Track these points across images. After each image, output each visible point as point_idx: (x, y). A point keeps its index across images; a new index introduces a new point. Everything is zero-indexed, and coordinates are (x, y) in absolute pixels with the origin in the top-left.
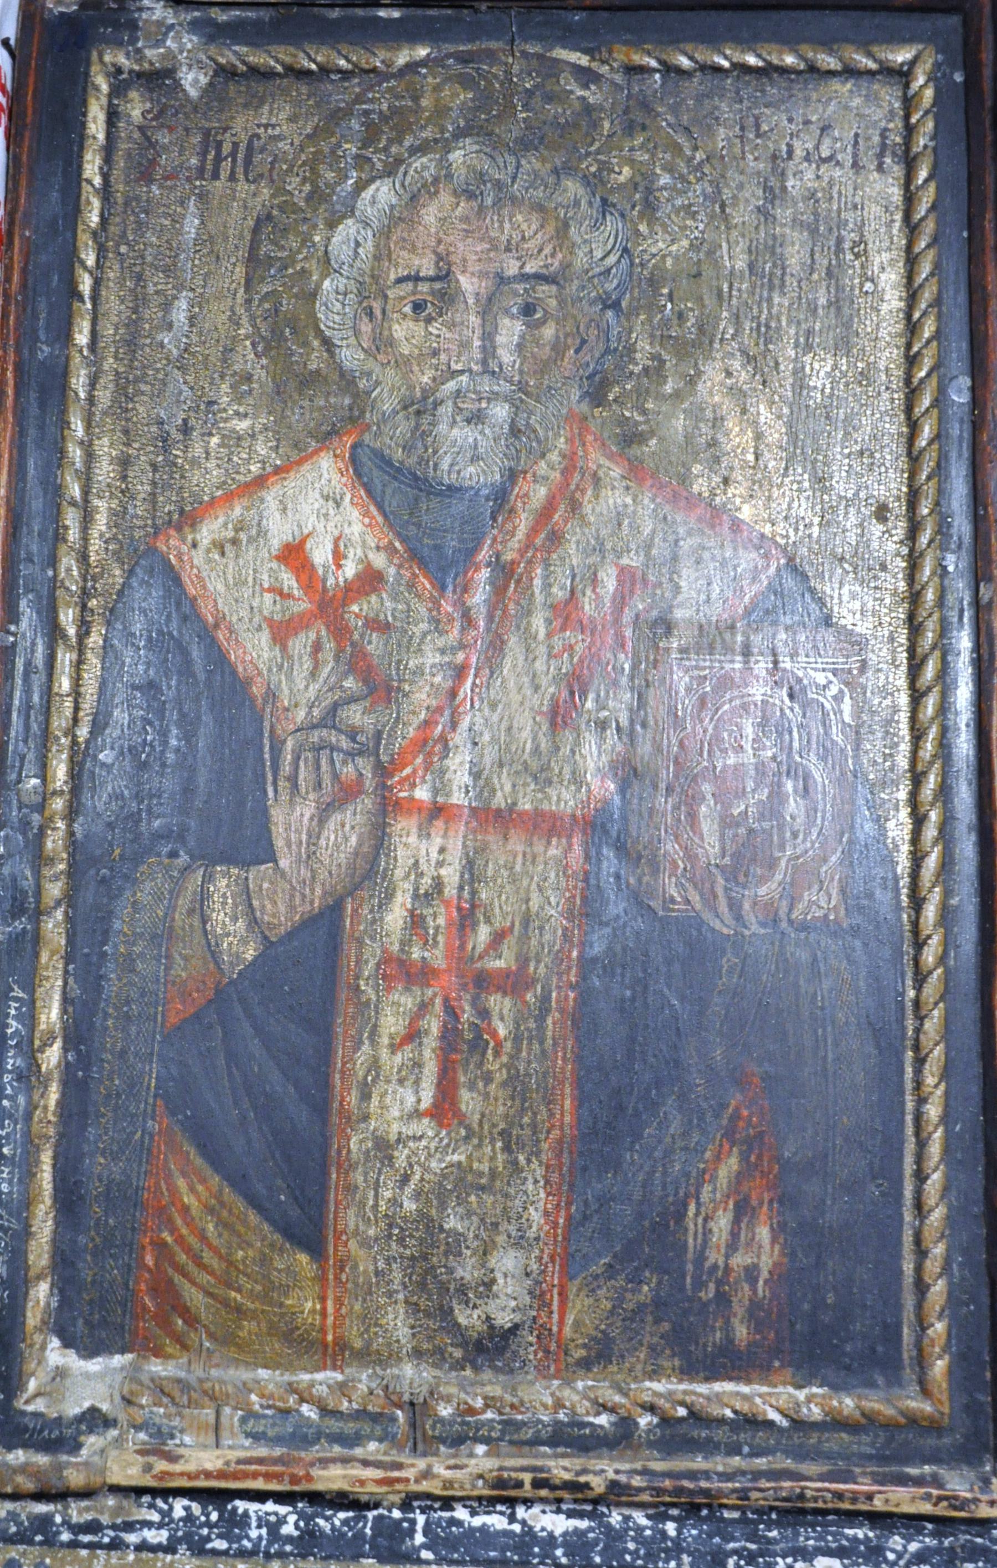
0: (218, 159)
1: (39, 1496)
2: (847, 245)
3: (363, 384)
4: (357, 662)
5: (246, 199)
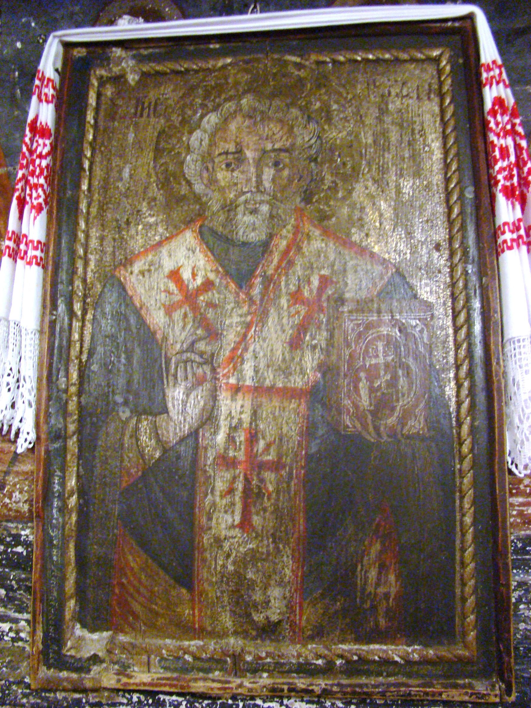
0: (143, 109)
1: (75, 690)
2: (416, 132)
3: (204, 199)
4: (203, 322)
5: (154, 125)
